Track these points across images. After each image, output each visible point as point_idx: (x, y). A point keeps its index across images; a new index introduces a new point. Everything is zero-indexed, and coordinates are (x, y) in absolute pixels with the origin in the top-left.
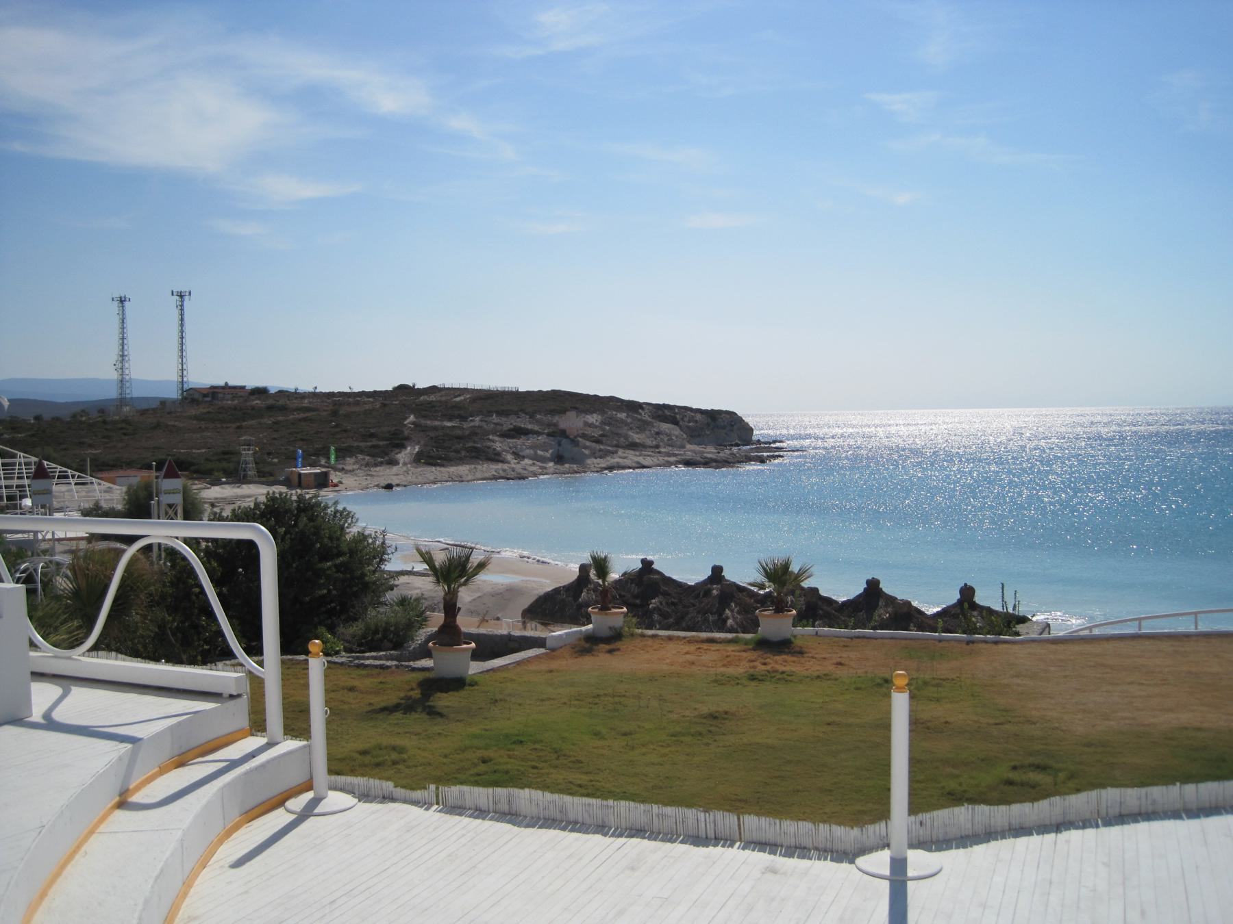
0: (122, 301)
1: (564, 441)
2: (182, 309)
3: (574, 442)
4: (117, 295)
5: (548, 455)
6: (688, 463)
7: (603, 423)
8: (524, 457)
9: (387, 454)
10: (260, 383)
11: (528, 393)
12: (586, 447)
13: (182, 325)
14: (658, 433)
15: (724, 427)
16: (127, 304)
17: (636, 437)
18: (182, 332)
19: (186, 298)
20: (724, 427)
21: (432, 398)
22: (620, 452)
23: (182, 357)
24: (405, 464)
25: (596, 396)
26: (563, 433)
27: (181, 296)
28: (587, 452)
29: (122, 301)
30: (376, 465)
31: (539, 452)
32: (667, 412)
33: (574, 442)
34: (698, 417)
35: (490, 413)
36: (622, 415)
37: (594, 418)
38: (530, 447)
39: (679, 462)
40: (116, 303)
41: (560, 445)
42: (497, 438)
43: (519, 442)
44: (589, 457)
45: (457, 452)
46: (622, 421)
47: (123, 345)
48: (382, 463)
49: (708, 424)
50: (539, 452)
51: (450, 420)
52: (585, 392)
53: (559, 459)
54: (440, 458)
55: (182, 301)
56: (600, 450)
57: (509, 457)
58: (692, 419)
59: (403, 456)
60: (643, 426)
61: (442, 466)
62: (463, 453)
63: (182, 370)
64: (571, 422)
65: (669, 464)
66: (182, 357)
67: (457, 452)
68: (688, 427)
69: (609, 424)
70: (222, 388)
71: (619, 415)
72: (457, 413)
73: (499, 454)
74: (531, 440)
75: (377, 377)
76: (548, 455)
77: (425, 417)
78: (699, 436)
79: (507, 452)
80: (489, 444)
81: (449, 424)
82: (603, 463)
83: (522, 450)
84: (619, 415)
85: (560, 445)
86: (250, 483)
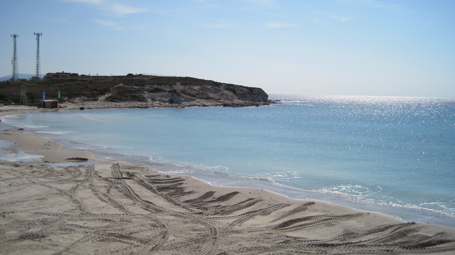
0: (15, 36)
1: (175, 95)
2: (38, 40)
3: (179, 95)
4: (13, 34)
5: (167, 100)
6: (225, 105)
7: (200, 89)
8: (156, 100)
9: (95, 97)
10: (75, 72)
11: (217, 82)
12: (183, 97)
13: (38, 47)
14: (222, 94)
15: (256, 94)
16: (17, 38)
17: (211, 95)
18: (38, 49)
19: (40, 36)
20: (256, 94)
21: (139, 78)
22: (197, 100)
23: (38, 59)
24: (101, 101)
25: (180, 77)
26: (175, 91)
27: (15, 36)
28: (183, 99)
29: (38, 35)
30: (88, 101)
31: (163, 99)
32: (232, 87)
33: (179, 95)
34: (245, 90)
35: (154, 84)
36: (209, 87)
37: (196, 88)
38: (160, 97)
39: (222, 105)
40: (13, 37)
41: (173, 96)
42: (147, 92)
43: (156, 94)
44: (183, 101)
45: (127, 97)
46: (209, 89)
47: (15, 54)
48: (91, 100)
49: (249, 93)
50: (163, 99)
51: (137, 86)
52: (199, 78)
53: (171, 102)
54: (117, 99)
55: (38, 37)
56: (189, 99)
57: (149, 100)
58: (242, 90)
59: (102, 98)
60: (216, 91)
61: (117, 102)
62: (129, 97)
63: (38, 64)
64: (179, 87)
65: (217, 105)
66: (38, 59)
67: (127, 97)
68: (240, 93)
69: (201, 90)
70: (61, 73)
71: (208, 87)
72: (140, 83)
73: (144, 98)
74: (162, 93)
75: (121, 71)
76: (167, 100)
77: (126, 84)
78: (245, 97)
79: (149, 98)
80: (142, 94)
81: (127, 87)
82: (188, 104)
83: (156, 97)
84: (208, 87)
85: (173, 96)
86: (24, 105)
